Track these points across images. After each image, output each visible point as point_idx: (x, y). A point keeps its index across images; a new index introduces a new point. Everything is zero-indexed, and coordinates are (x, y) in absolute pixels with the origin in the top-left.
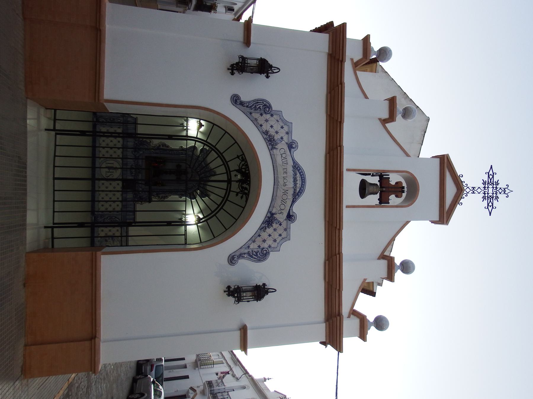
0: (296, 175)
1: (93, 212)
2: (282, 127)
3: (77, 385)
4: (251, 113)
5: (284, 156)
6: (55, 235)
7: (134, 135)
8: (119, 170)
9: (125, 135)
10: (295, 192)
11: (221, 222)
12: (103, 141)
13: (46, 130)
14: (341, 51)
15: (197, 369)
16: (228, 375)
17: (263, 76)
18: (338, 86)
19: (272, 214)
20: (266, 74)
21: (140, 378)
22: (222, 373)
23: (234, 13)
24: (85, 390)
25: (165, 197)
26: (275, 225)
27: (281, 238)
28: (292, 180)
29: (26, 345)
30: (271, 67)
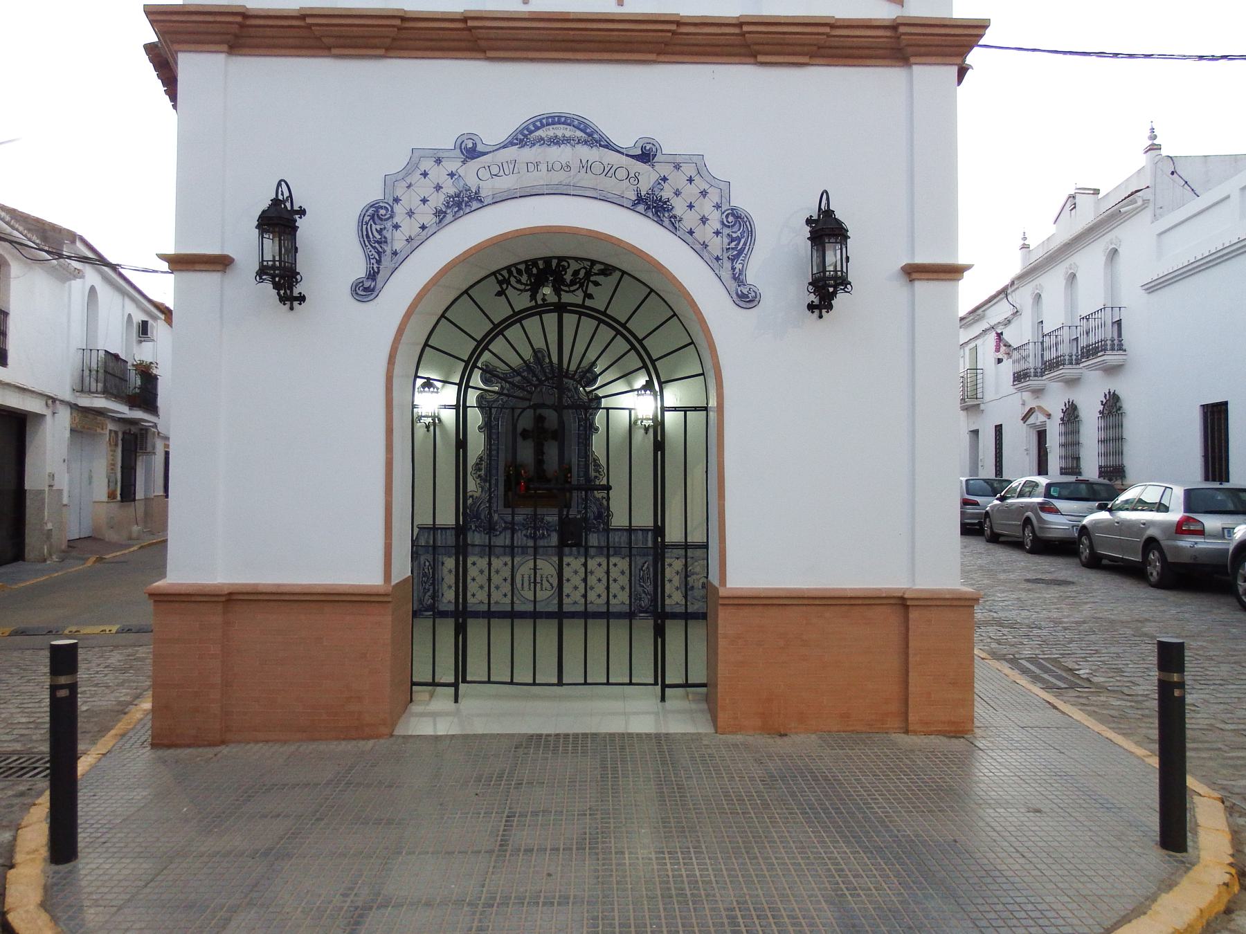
0: (542, 139)
1: (630, 616)
2: (425, 174)
3: (994, 645)
4: (395, 253)
5: (495, 170)
6: (681, 681)
7: (460, 530)
8: (538, 562)
9: (461, 551)
10: (586, 142)
11: (654, 328)
12: (477, 597)
13: (456, 701)
14: (219, 19)
15: (982, 407)
16: (1005, 336)
17: (300, 222)
18: (309, 26)
19: (640, 200)
20: (297, 217)
21: (991, 528)
22: (998, 350)
23: (151, 322)
24: (1005, 631)
25: (597, 465)
26: (667, 194)
27: (697, 179)
28: (554, 148)
29: (907, 732)
30: (276, 202)
